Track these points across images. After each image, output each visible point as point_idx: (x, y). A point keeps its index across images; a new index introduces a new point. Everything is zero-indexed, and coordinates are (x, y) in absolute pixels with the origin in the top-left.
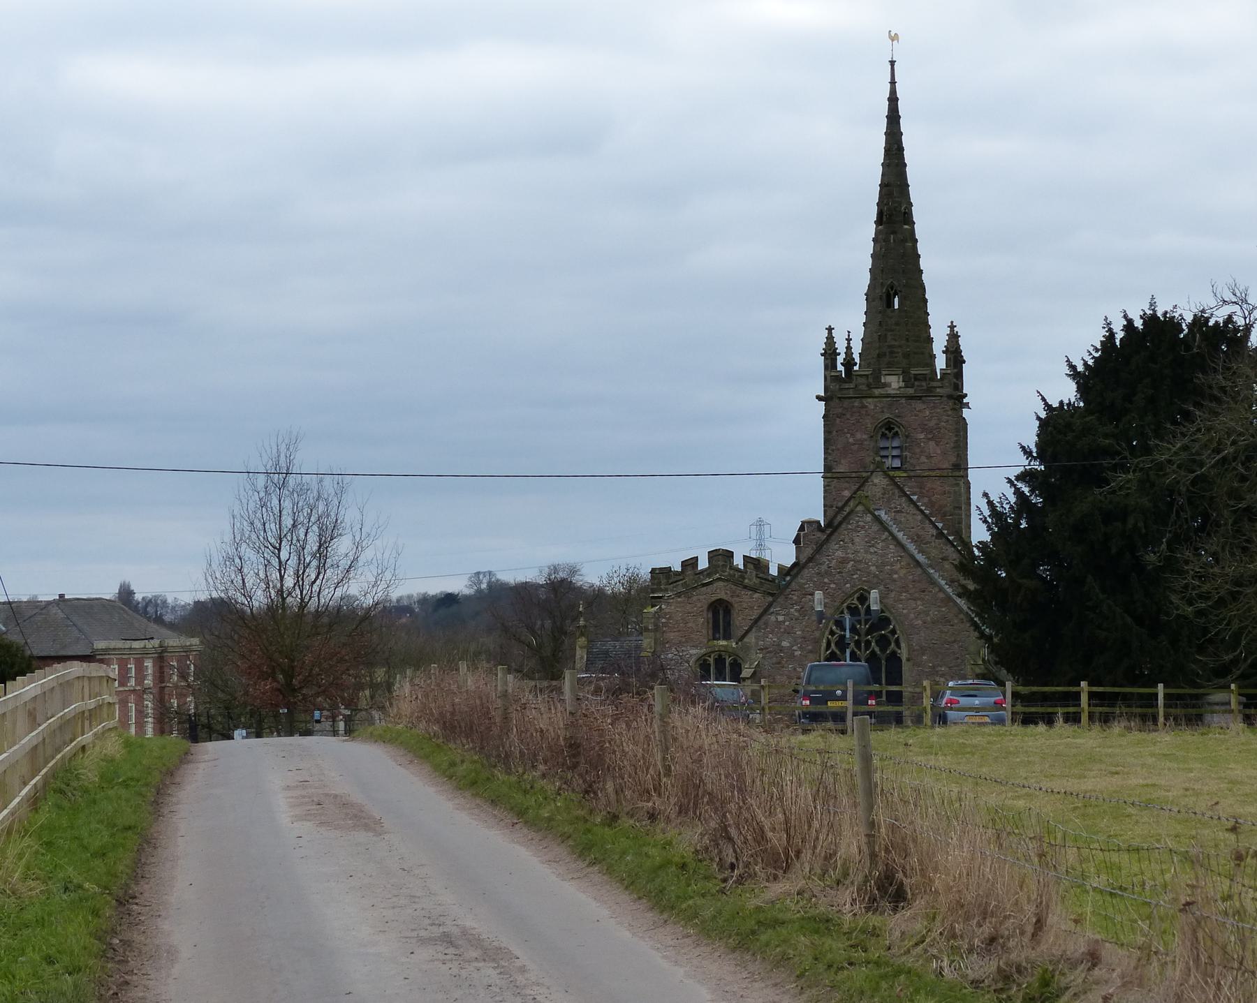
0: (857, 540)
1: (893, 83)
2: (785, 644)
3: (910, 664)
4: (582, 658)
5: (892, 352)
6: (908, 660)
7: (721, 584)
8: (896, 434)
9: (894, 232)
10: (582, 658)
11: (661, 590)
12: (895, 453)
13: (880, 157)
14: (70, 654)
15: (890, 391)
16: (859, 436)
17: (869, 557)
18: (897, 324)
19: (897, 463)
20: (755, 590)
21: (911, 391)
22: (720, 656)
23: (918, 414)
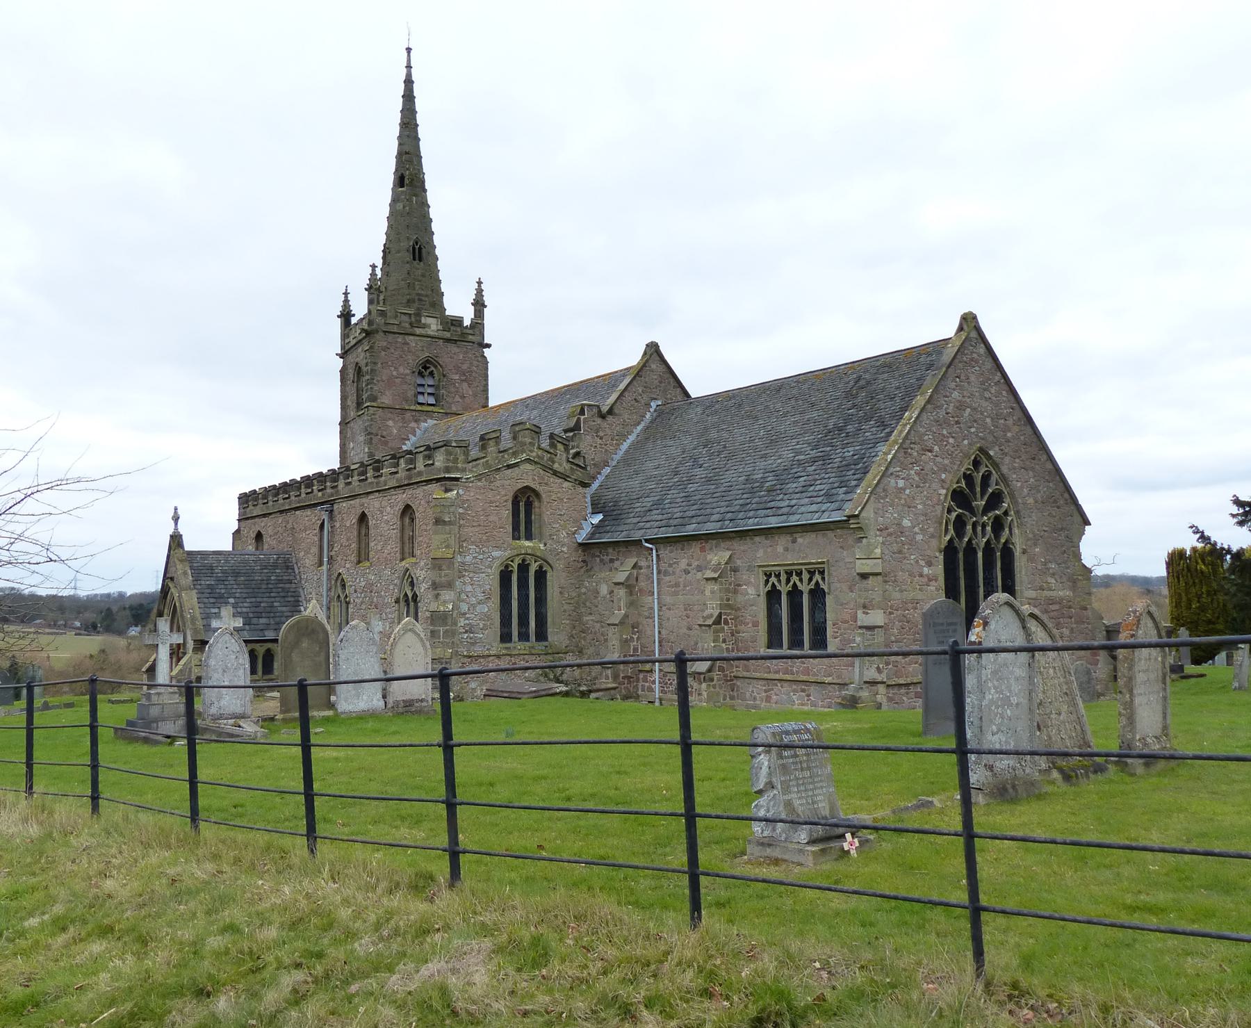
0: (973, 378)
1: (409, 67)
2: (906, 523)
3: (1024, 558)
4: (185, 573)
5: (420, 300)
6: (1024, 552)
7: (528, 466)
8: (431, 374)
9: (415, 195)
10: (185, 573)
11: (457, 470)
12: (430, 390)
13: (396, 131)
14: (441, 775)
15: (430, 333)
16: (401, 370)
17: (985, 404)
18: (423, 276)
19: (432, 400)
20: (564, 477)
21: (447, 335)
22: (524, 560)
23: (450, 357)
